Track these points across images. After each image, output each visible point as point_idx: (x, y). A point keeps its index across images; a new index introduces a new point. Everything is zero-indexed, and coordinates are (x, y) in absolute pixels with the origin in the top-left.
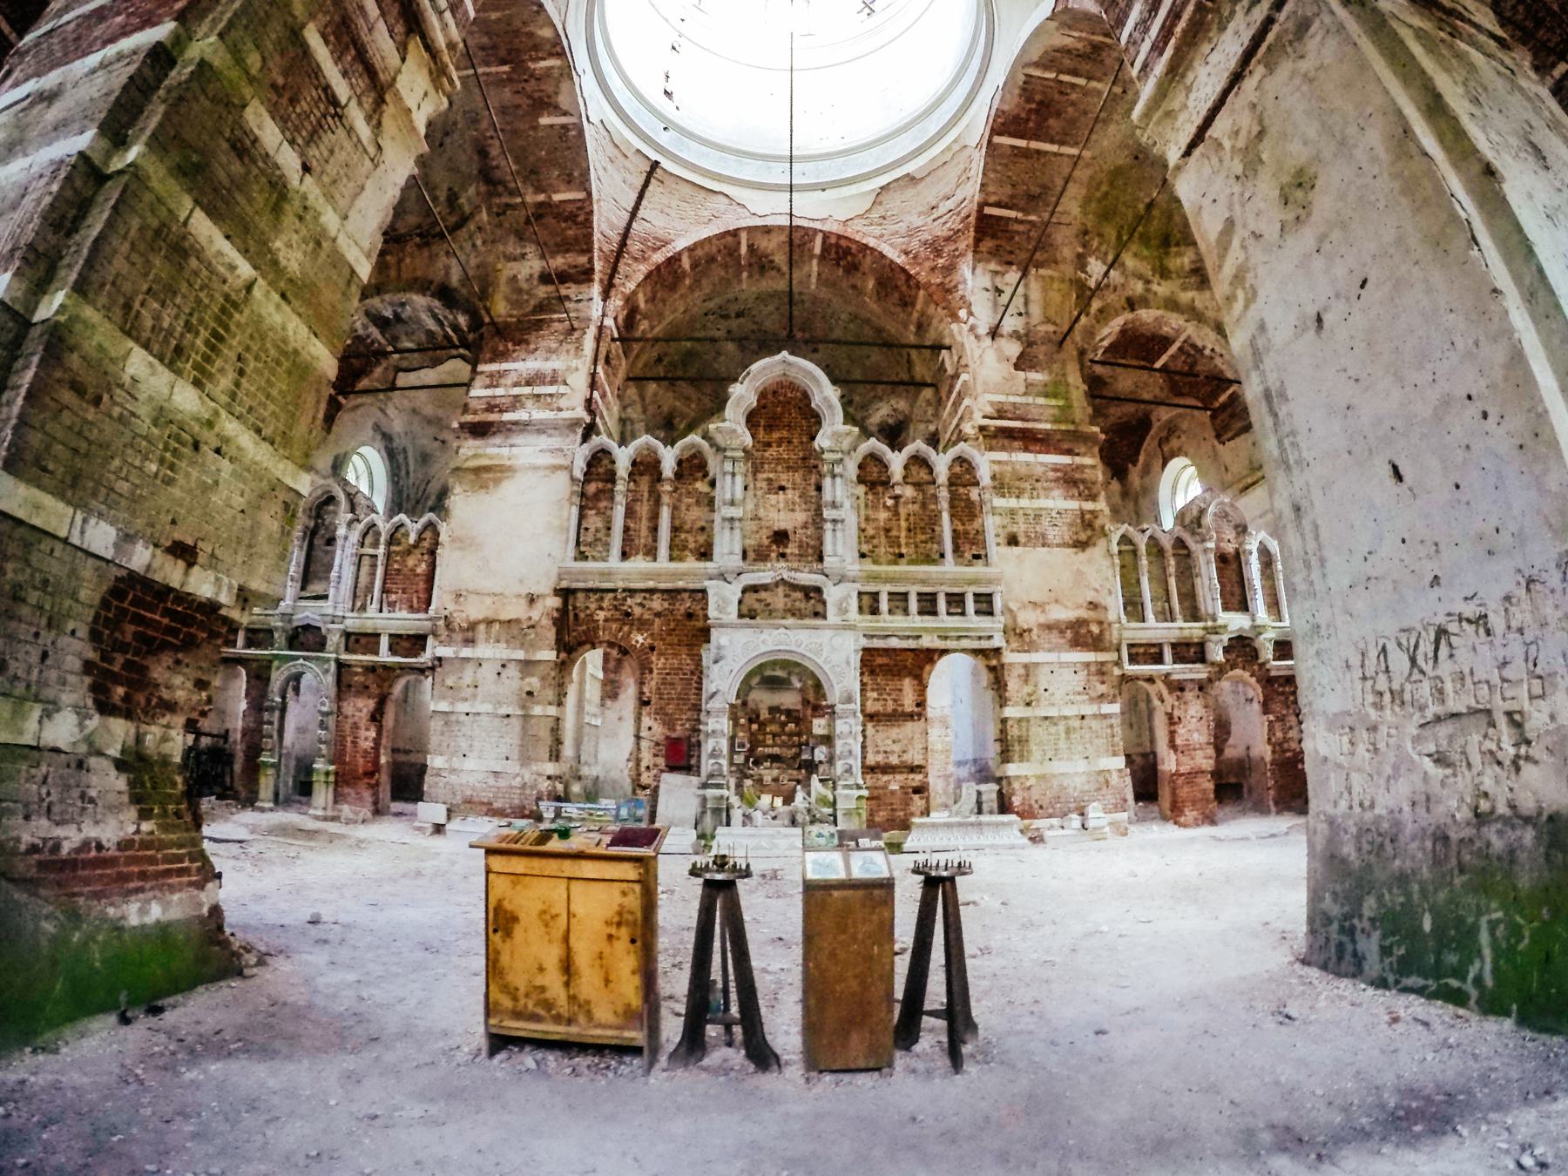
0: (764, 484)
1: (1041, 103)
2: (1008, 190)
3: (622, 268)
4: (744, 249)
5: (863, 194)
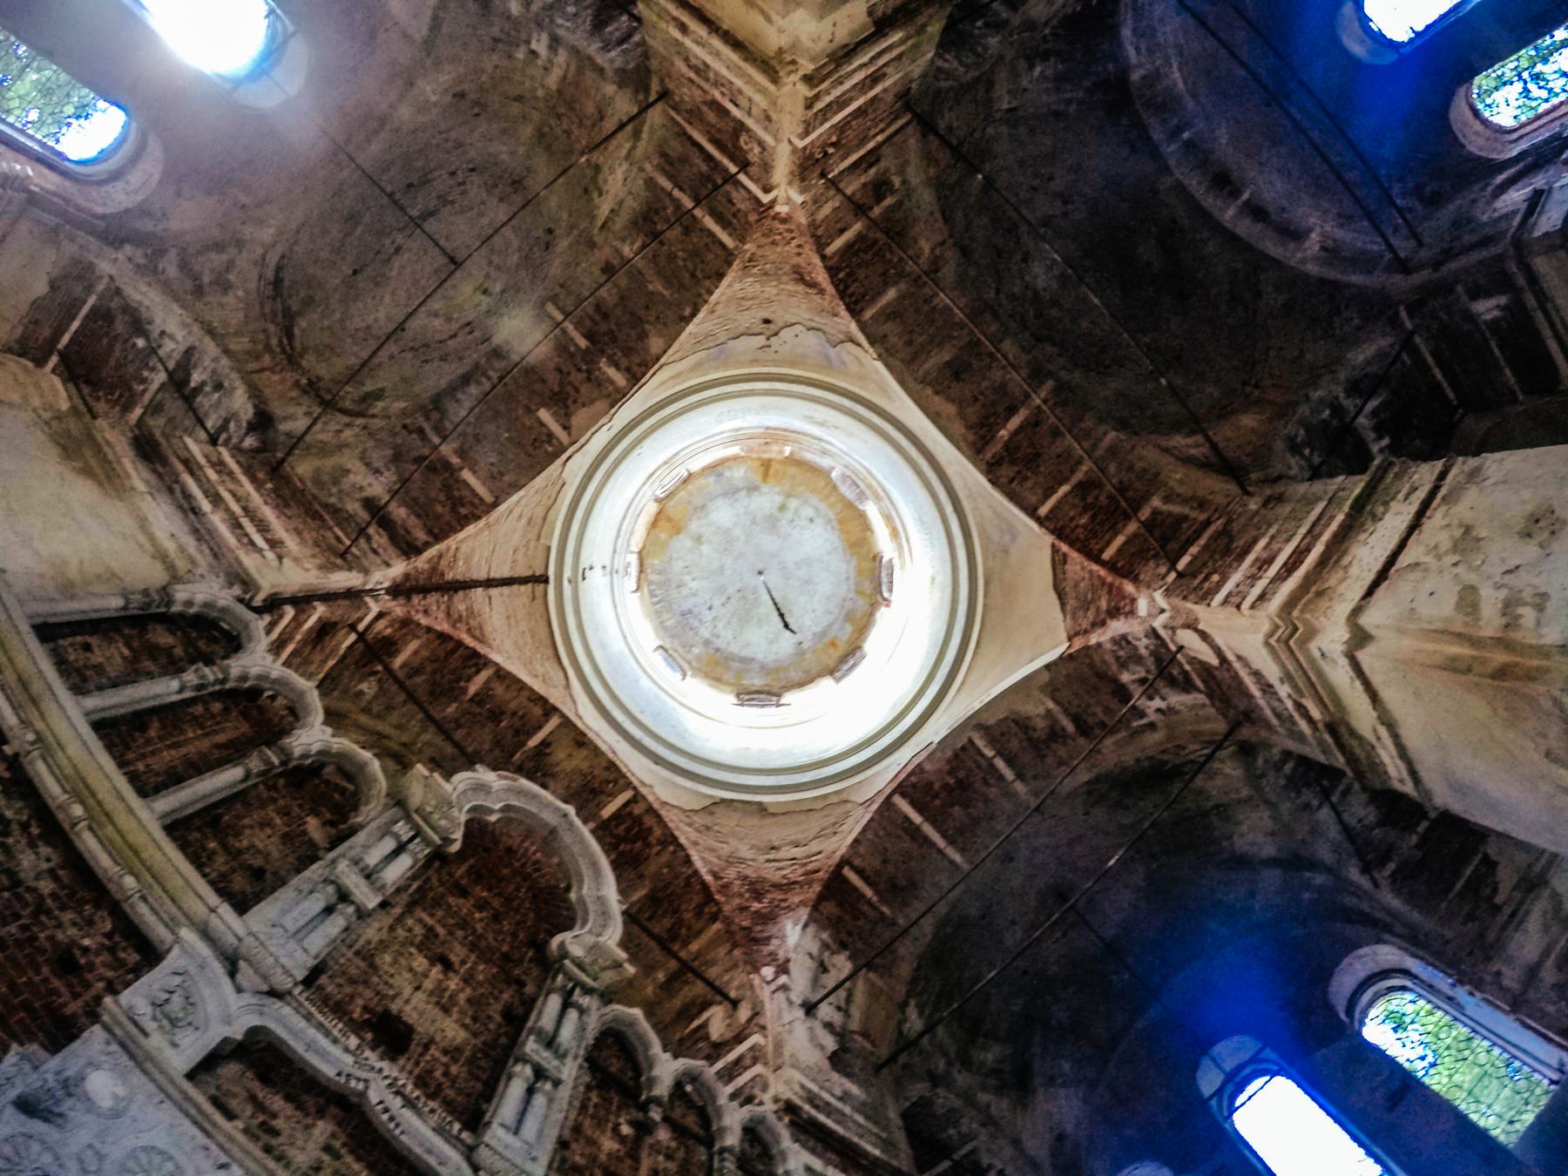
0: (419, 930)
1: (959, 782)
2: (876, 863)
3: (432, 598)
4: (534, 742)
5: (698, 794)
